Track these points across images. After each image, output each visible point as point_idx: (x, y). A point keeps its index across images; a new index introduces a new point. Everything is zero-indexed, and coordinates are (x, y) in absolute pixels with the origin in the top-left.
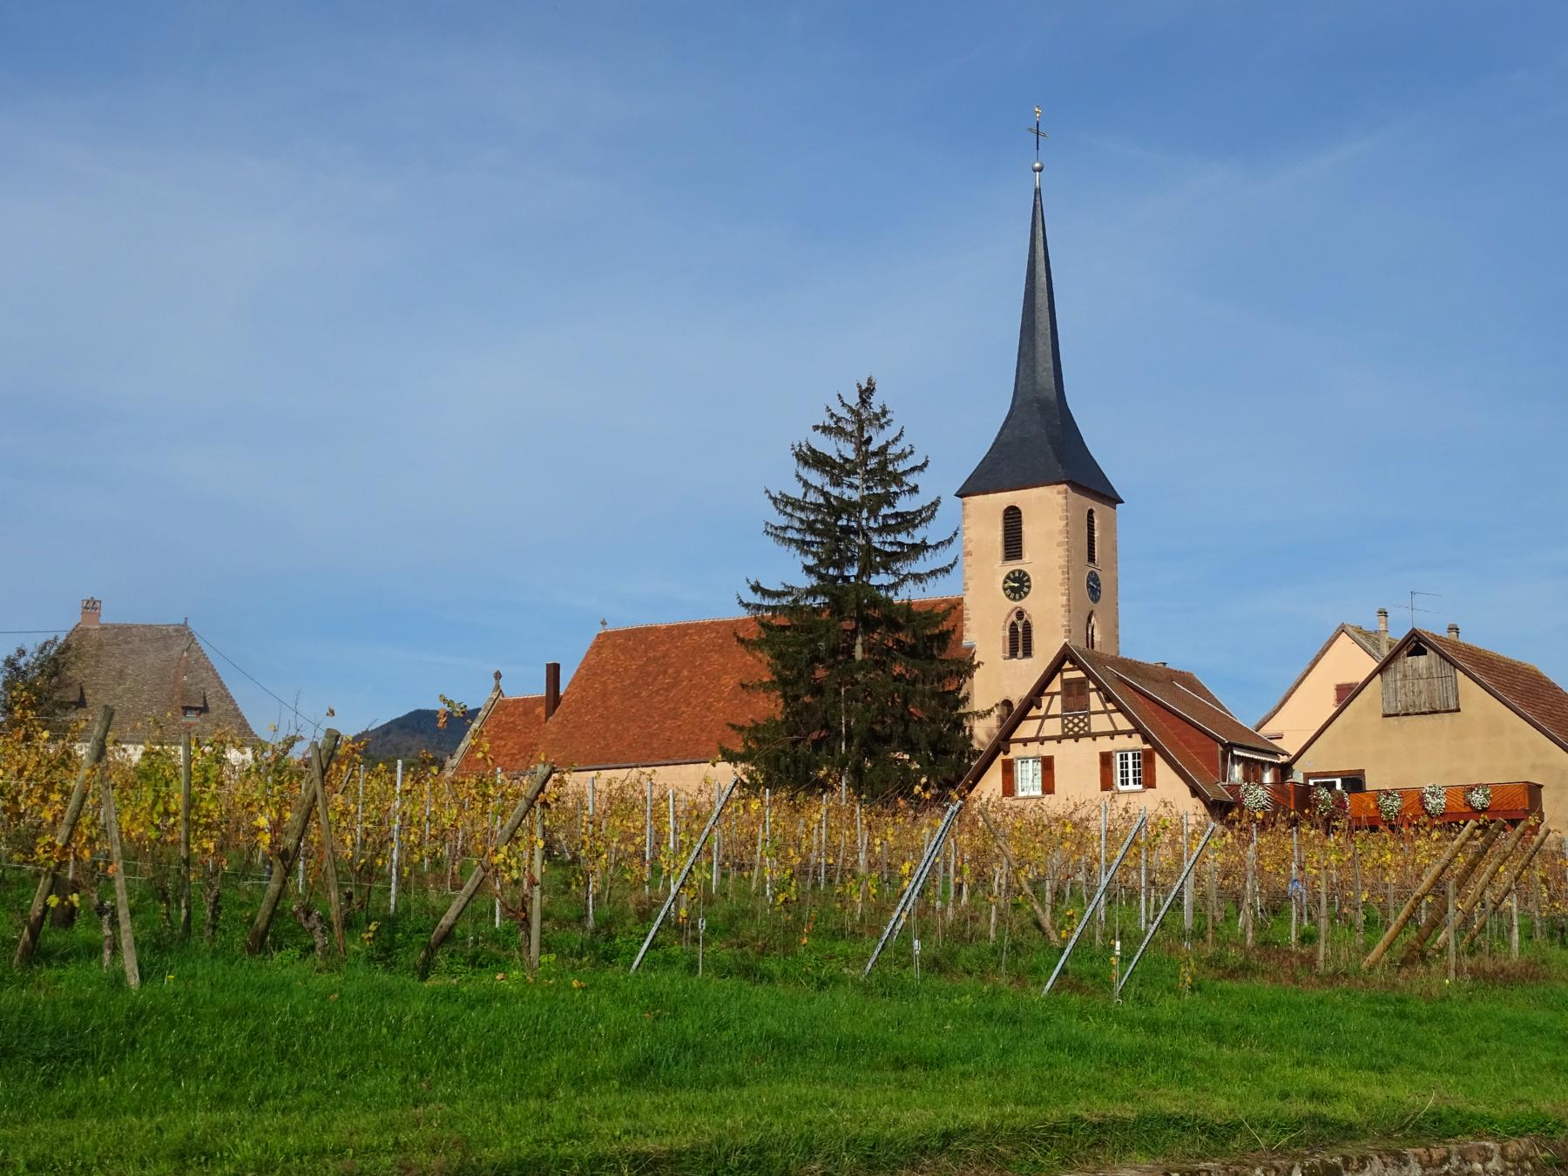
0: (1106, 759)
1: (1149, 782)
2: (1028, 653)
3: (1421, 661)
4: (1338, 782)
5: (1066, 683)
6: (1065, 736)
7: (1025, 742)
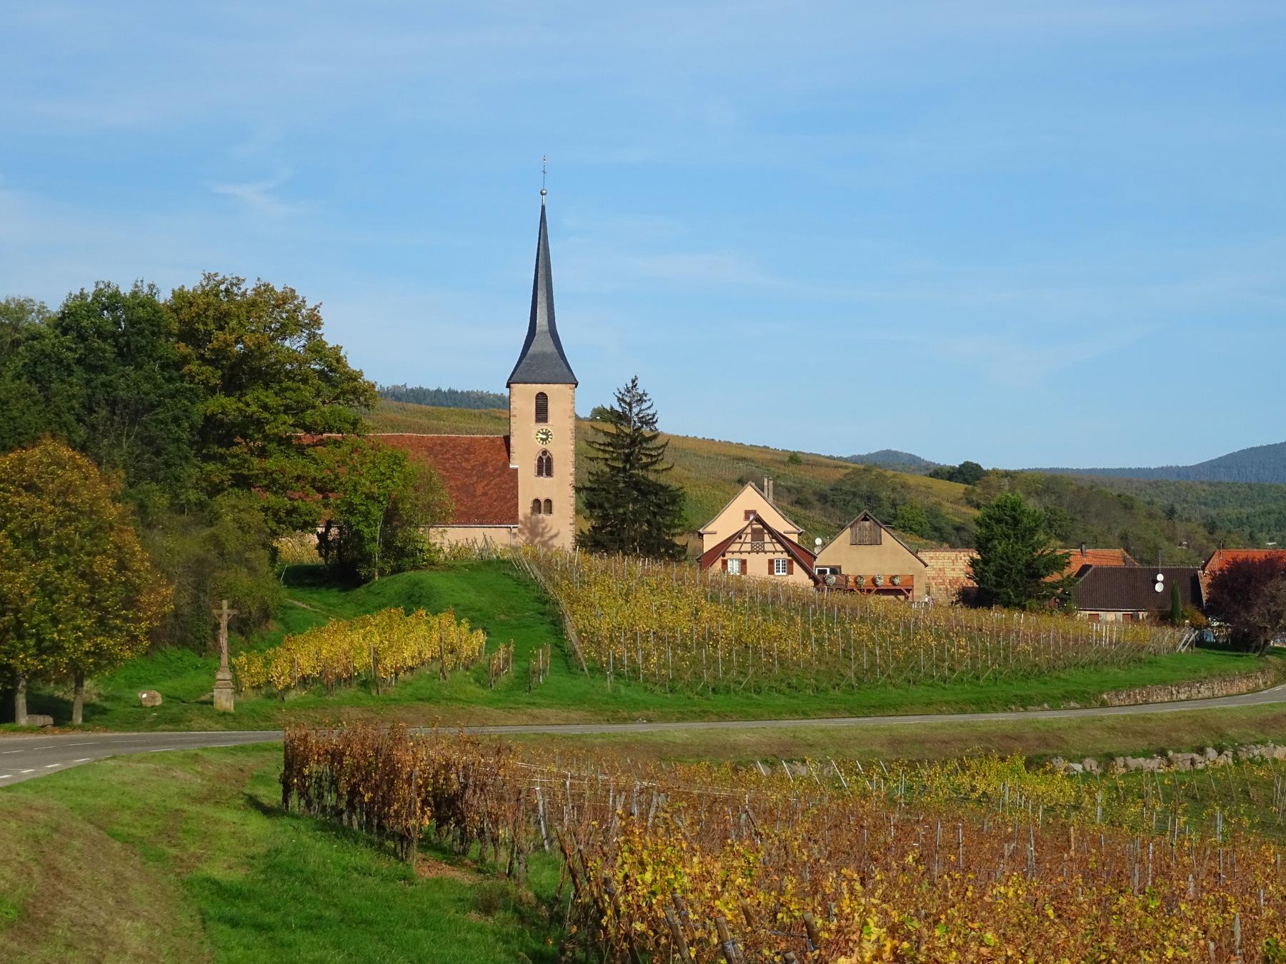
0: (771, 562)
1: (790, 572)
2: (549, 474)
3: (867, 523)
4: (828, 570)
5: (753, 529)
6: (752, 551)
7: (733, 552)
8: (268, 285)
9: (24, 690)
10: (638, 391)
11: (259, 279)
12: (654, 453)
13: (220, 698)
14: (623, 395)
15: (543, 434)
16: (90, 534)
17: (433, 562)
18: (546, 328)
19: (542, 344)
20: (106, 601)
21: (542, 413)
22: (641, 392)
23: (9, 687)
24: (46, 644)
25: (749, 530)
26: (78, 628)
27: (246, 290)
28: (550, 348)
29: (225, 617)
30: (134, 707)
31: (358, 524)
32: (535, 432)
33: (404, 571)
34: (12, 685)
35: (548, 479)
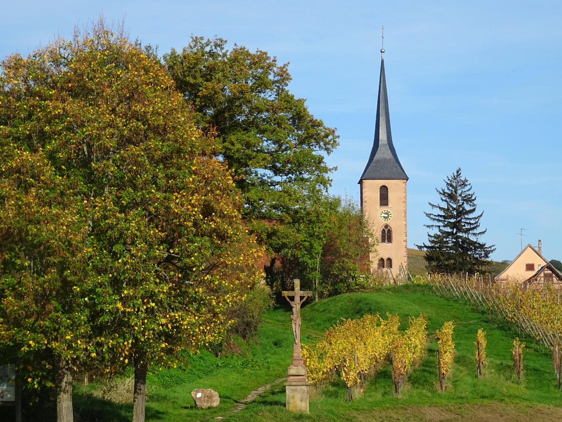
2: (390, 241)
8: (244, 48)
9: (69, 388)
10: (461, 178)
11: (235, 45)
12: (473, 222)
13: (293, 397)
14: (451, 181)
15: (385, 214)
16: (165, 160)
17: (363, 286)
18: (386, 142)
19: (383, 153)
20: (189, 256)
21: (384, 199)
22: (463, 179)
23: (49, 384)
24: (106, 318)
25: (542, 275)
26: (152, 296)
27: (227, 51)
28: (388, 155)
29: (297, 299)
30: (186, 408)
31: (303, 256)
32: (380, 213)
33: (340, 293)
34: (53, 381)
35: (390, 244)
